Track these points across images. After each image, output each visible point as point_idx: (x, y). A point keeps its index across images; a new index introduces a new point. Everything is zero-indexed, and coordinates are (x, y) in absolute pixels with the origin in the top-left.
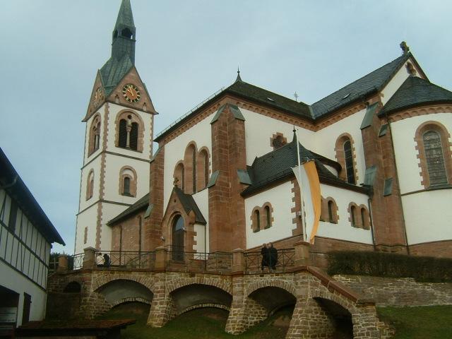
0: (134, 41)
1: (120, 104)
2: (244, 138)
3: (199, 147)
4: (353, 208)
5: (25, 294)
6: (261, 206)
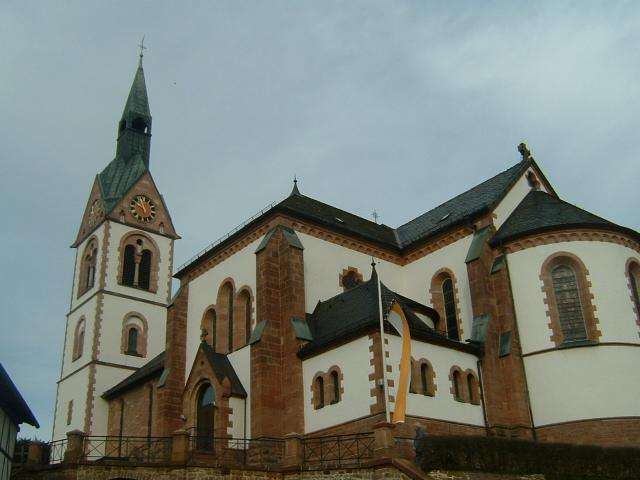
0: (149, 135)
4: (456, 374)
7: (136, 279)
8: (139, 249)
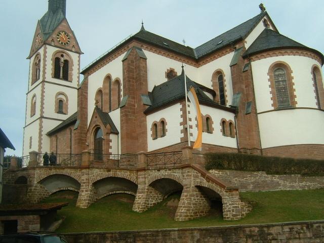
4: (223, 122)
7: (61, 75)
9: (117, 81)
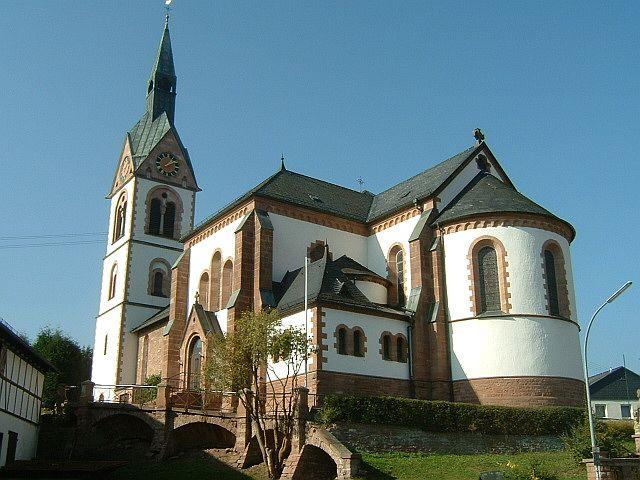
0: (174, 94)
1: (153, 179)
2: (272, 252)
3: (224, 259)
4: (386, 339)
5: (10, 432)
6: (351, 327)
7: (161, 229)
8: (164, 201)
9: (229, 264)
